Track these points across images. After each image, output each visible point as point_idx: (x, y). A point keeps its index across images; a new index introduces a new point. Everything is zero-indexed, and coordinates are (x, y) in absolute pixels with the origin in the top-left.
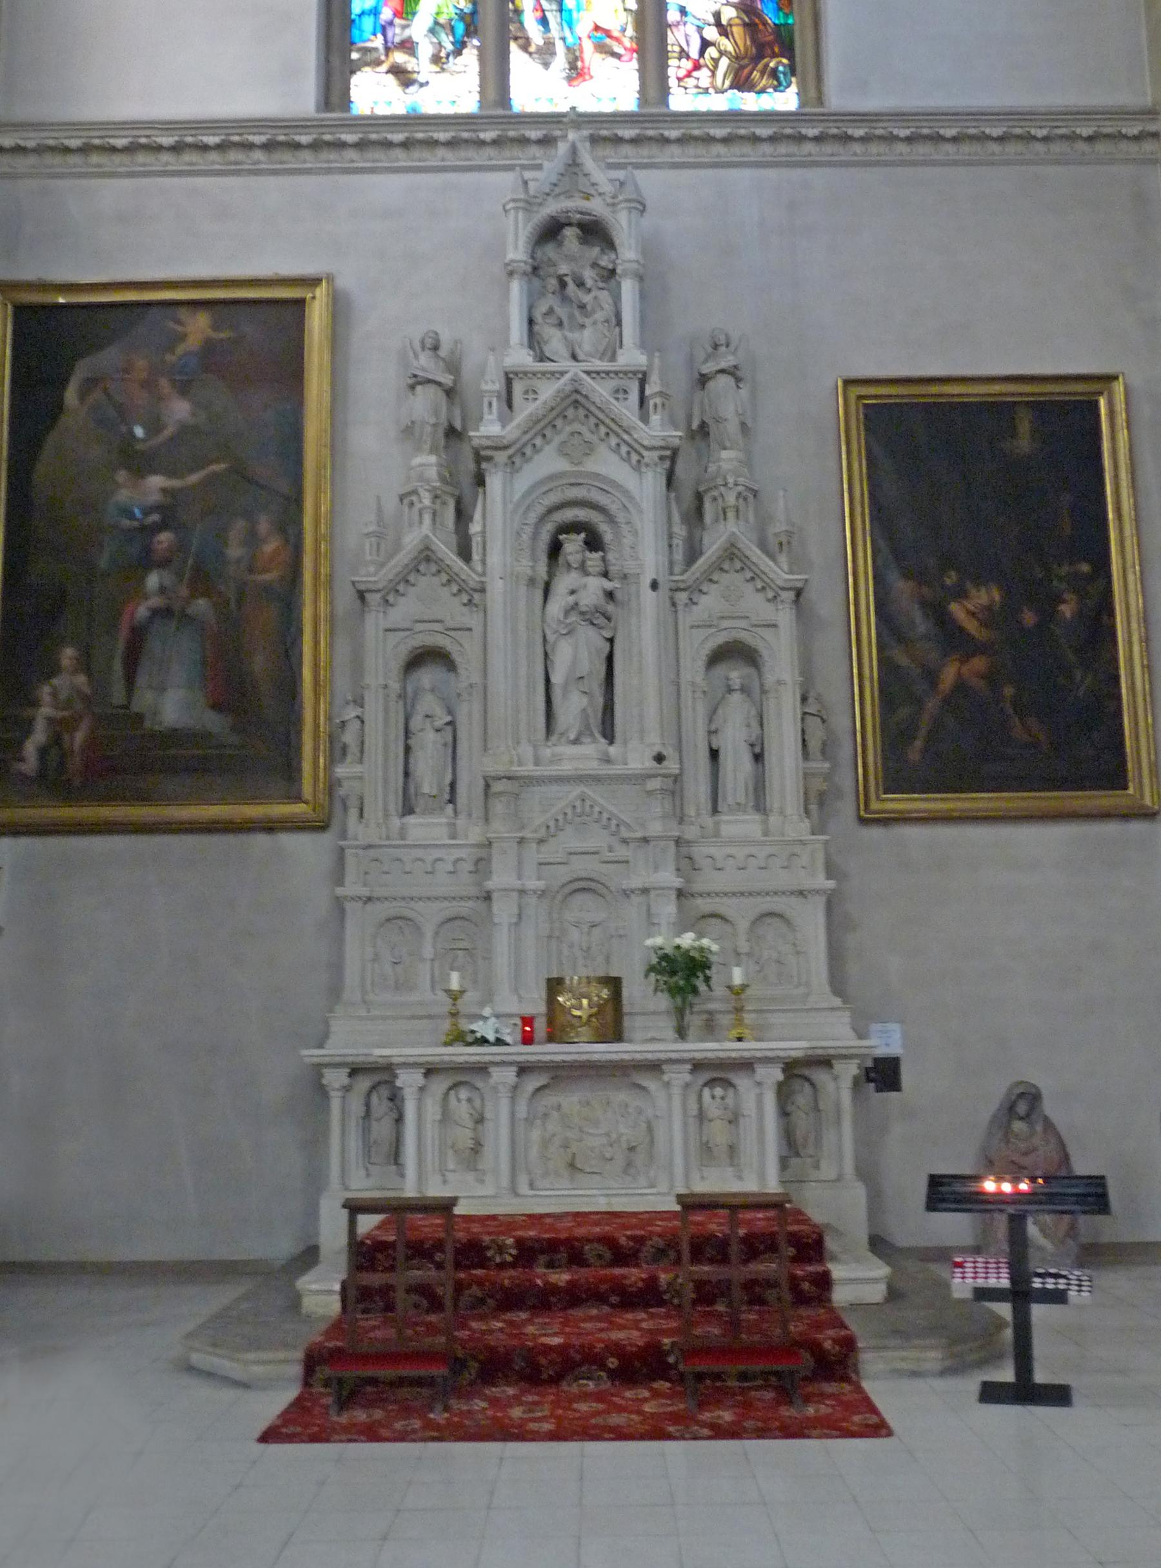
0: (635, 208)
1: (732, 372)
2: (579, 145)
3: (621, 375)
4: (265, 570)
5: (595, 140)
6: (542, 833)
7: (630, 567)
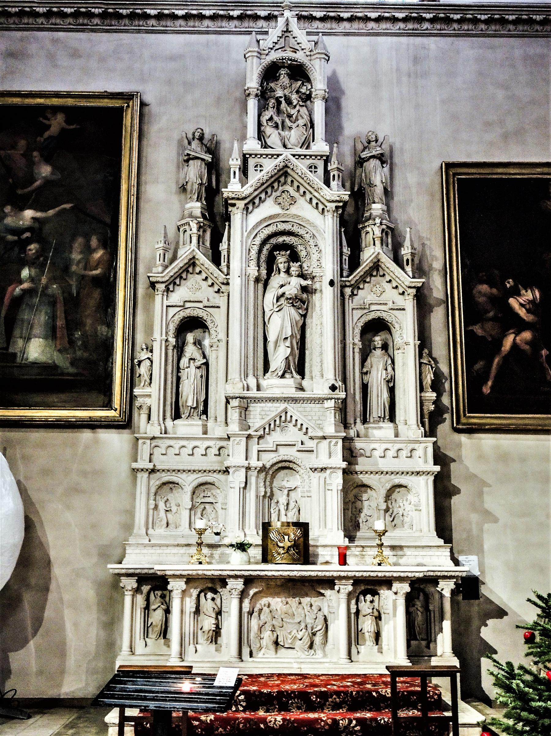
0: (324, 58)
1: (381, 158)
2: (290, 19)
3: (313, 157)
4: (96, 268)
5: (300, 18)
6: (261, 432)
7: (317, 272)
